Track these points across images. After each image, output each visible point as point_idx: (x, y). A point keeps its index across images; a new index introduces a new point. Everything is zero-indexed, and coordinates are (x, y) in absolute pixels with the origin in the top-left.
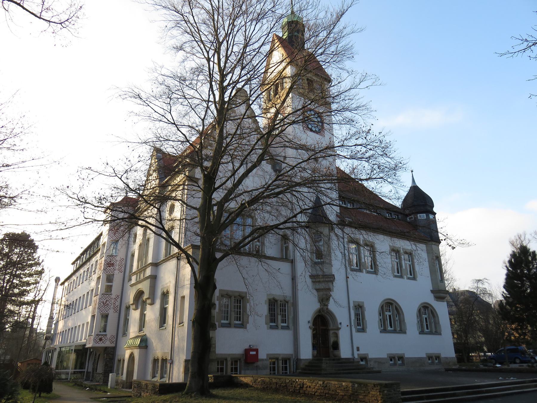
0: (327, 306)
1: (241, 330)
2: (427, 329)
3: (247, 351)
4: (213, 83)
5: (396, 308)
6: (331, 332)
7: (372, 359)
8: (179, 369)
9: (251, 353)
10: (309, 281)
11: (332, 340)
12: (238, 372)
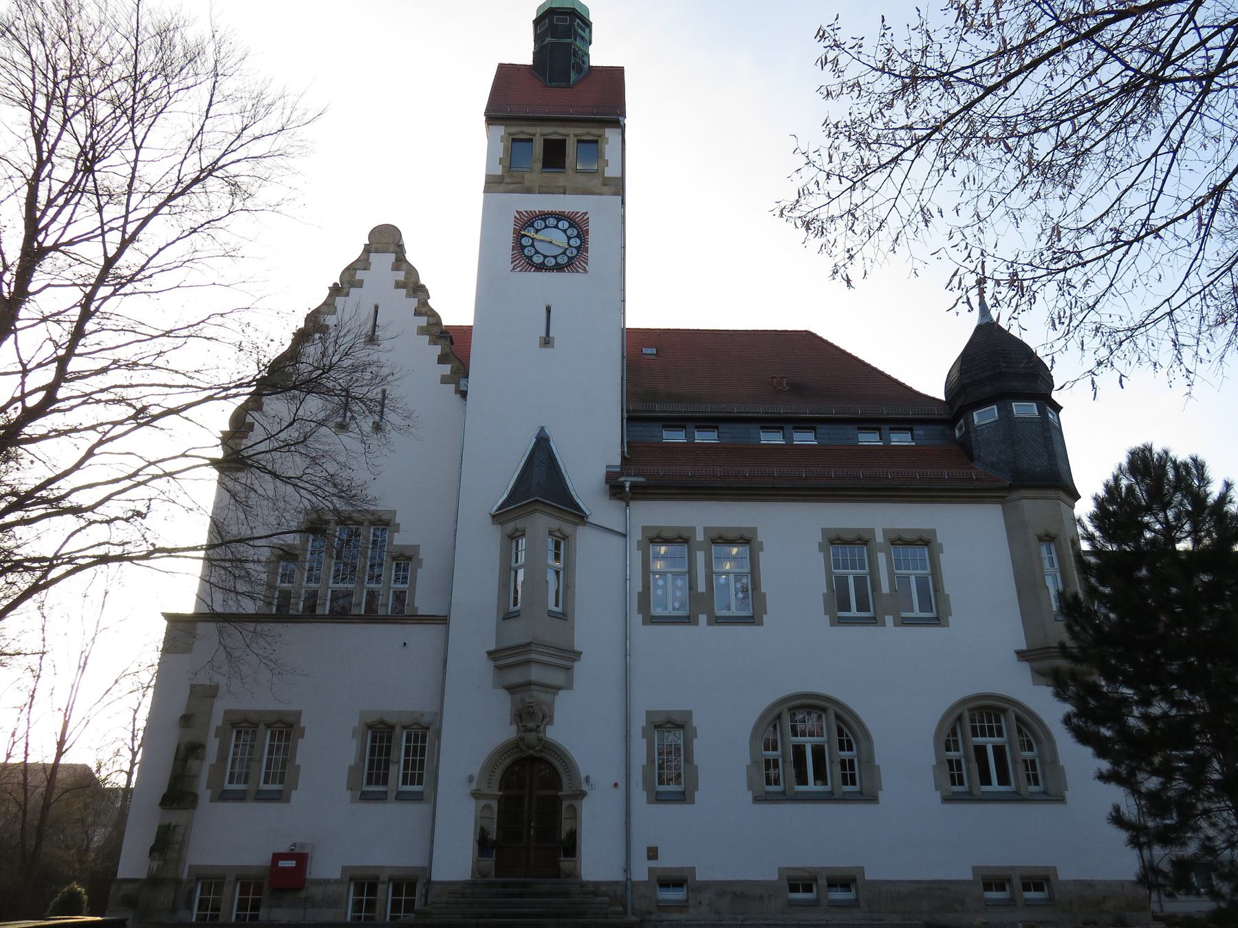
4: (1028, 60)
5: (838, 717)
6: (565, 804)
9: (282, 864)
11: (566, 827)
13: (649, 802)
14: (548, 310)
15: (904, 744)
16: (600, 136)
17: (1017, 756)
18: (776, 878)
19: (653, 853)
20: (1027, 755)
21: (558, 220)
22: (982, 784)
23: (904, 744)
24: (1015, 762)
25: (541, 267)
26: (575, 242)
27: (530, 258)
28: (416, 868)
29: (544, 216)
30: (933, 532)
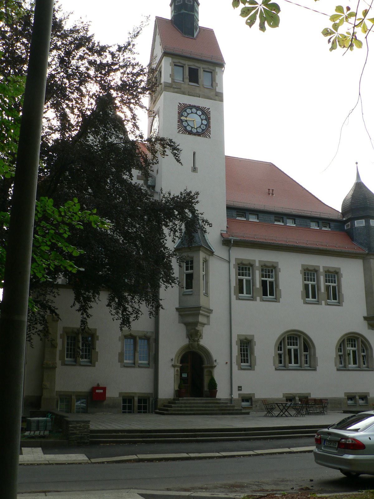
0: (198, 341)
1: (313, 372)
2: (364, 364)
3: (94, 389)
5: (362, 342)
7: (258, 400)
8: (245, 405)
9: (97, 391)
10: (175, 315)
12: (148, 411)
13: (238, 370)
14: (194, 154)
15: (326, 350)
16: (213, 70)
17: (302, 354)
18: (282, 397)
19: (240, 388)
20: (363, 354)
21: (197, 110)
22: (289, 363)
23: (326, 350)
24: (359, 356)
25: (190, 133)
26: (205, 122)
27: (185, 127)
28: (149, 393)
29: (191, 107)
30: (339, 269)
